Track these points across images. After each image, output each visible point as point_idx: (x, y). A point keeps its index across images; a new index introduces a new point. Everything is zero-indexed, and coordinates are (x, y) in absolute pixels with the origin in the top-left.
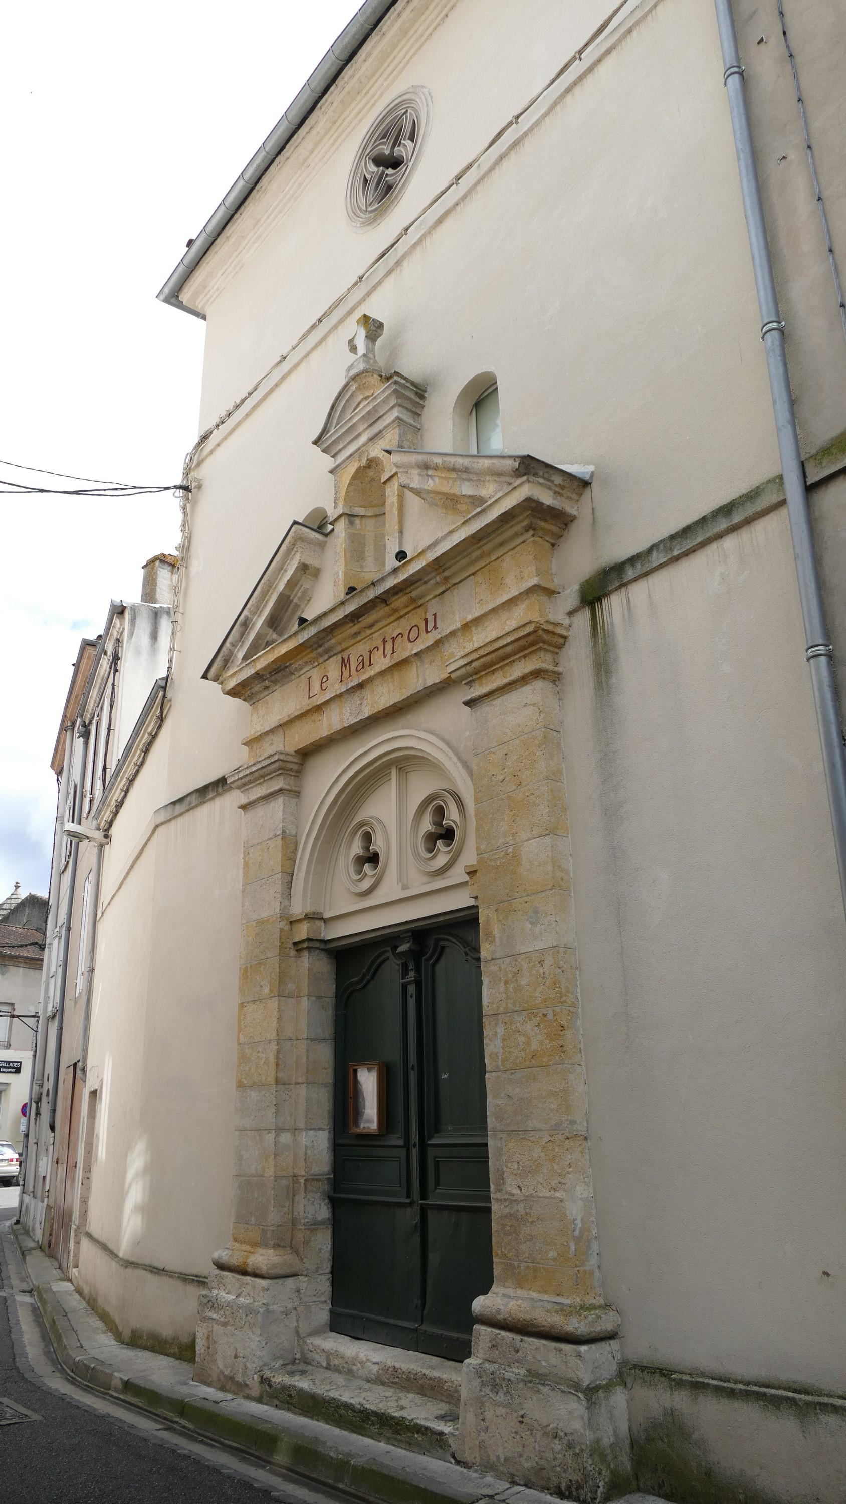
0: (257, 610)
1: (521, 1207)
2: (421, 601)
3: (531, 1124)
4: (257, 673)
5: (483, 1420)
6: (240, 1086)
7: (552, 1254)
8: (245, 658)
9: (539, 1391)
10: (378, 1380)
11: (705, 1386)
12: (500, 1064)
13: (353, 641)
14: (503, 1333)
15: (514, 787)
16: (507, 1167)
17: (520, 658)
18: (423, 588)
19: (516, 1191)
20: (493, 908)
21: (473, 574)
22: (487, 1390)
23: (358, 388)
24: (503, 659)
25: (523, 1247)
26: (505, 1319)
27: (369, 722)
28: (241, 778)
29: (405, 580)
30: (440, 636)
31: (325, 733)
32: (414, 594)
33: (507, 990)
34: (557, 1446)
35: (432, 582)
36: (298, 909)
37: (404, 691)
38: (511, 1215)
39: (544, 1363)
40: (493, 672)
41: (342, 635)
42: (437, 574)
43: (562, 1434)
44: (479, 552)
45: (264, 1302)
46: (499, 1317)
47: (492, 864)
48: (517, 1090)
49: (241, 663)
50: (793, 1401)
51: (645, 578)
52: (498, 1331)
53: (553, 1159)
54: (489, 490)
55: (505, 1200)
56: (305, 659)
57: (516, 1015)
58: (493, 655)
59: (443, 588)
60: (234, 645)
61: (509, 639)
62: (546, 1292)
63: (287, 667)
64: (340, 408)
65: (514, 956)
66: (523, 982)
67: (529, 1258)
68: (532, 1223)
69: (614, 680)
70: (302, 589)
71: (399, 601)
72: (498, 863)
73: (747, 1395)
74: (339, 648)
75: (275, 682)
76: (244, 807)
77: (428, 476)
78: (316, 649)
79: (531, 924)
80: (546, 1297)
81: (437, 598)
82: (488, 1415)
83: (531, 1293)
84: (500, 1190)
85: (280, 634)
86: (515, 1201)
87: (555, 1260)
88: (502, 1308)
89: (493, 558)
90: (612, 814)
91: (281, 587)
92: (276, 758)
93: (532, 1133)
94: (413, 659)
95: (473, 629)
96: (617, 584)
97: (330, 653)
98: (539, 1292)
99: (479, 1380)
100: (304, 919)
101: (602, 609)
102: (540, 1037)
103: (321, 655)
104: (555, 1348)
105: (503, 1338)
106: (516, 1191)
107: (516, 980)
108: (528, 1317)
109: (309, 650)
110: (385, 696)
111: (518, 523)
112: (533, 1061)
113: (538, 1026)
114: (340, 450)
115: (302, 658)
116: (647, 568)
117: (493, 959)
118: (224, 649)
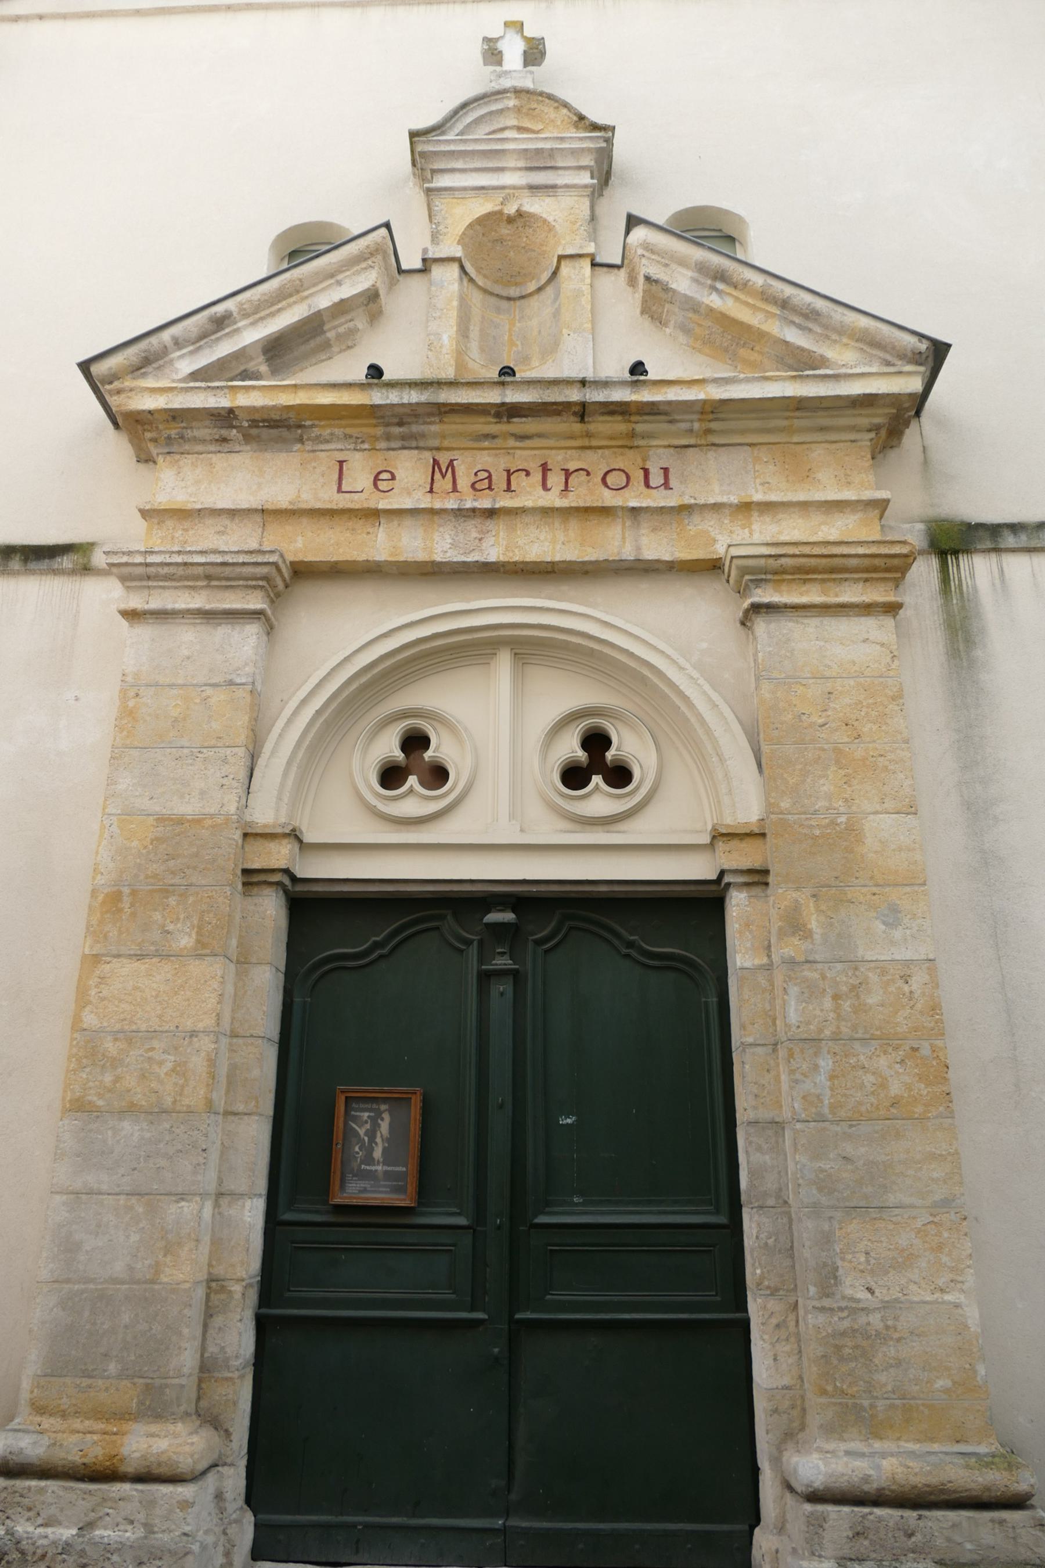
0: (257, 312)
2: (641, 443)
3: (891, 1199)
4: (231, 411)
6: (78, 1107)
8: (194, 376)
12: (826, 1111)
13: (471, 444)
14: (878, 1511)
15: (846, 740)
16: (843, 1259)
17: (859, 580)
18: (665, 426)
19: (863, 1295)
21: (750, 445)
23: (518, 110)
24: (833, 570)
26: (879, 1490)
28: (147, 565)
29: (653, 403)
30: (693, 501)
31: (359, 555)
32: (640, 428)
33: (837, 1009)
35: (683, 426)
36: (265, 813)
37: (590, 550)
38: (854, 1331)
39: (969, 1546)
40: (805, 581)
41: (460, 427)
42: (700, 420)
44: (785, 423)
45: (187, 1529)
46: (866, 1488)
47: (805, 831)
48: (863, 1150)
49: (183, 380)
51: (1027, 554)
53: (940, 1247)
54: (843, 356)
55: (841, 1309)
56: (348, 431)
57: (857, 1045)
58: (824, 561)
59: (692, 441)
60: (178, 343)
61: (861, 550)
62: (932, 1440)
63: (300, 426)
64: (469, 119)
65: (854, 964)
67: (894, 1392)
68: (899, 1340)
69: (978, 653)
70: (351, 325)
71: (602, 426)
72: (817, 832)
74: (436, 443)
75: (248, 438)
76: (132, 615)
77: (716, 290)
78: (387, 425)
79: (884, 923)
80: (936, 1447)
81: (672, 450)
83: (902, 1443)
85: (275, 372)
86: (863, 1309)
87: (947, 1391)
88: (872, 1472)
89: (795, 439)
90: (978, 812)
91: (324, 301)
92: (272, 559)
93: (897, 1211)
94: (620, 514)
95: (756, 514)
96: (989, 545)
97: (410, 442)
98: (919, 1441)
100: (286, 835)
101: (958, 565)
102: (907, 1079)
103: (388, 437)
104: (992, 1521)
105: (880, 1519)
106: (863, 1295)
107: (858, 996)
108: (934, 1480)
109: (374, 421)
110: (539, 545)
111: (868, 416)
112: (893, 1110)
113: (902, 1062)
114: (452, 170)
115: (345, 427)
116: (1034, 543)
117: (807, 962)
118: (153, 340)
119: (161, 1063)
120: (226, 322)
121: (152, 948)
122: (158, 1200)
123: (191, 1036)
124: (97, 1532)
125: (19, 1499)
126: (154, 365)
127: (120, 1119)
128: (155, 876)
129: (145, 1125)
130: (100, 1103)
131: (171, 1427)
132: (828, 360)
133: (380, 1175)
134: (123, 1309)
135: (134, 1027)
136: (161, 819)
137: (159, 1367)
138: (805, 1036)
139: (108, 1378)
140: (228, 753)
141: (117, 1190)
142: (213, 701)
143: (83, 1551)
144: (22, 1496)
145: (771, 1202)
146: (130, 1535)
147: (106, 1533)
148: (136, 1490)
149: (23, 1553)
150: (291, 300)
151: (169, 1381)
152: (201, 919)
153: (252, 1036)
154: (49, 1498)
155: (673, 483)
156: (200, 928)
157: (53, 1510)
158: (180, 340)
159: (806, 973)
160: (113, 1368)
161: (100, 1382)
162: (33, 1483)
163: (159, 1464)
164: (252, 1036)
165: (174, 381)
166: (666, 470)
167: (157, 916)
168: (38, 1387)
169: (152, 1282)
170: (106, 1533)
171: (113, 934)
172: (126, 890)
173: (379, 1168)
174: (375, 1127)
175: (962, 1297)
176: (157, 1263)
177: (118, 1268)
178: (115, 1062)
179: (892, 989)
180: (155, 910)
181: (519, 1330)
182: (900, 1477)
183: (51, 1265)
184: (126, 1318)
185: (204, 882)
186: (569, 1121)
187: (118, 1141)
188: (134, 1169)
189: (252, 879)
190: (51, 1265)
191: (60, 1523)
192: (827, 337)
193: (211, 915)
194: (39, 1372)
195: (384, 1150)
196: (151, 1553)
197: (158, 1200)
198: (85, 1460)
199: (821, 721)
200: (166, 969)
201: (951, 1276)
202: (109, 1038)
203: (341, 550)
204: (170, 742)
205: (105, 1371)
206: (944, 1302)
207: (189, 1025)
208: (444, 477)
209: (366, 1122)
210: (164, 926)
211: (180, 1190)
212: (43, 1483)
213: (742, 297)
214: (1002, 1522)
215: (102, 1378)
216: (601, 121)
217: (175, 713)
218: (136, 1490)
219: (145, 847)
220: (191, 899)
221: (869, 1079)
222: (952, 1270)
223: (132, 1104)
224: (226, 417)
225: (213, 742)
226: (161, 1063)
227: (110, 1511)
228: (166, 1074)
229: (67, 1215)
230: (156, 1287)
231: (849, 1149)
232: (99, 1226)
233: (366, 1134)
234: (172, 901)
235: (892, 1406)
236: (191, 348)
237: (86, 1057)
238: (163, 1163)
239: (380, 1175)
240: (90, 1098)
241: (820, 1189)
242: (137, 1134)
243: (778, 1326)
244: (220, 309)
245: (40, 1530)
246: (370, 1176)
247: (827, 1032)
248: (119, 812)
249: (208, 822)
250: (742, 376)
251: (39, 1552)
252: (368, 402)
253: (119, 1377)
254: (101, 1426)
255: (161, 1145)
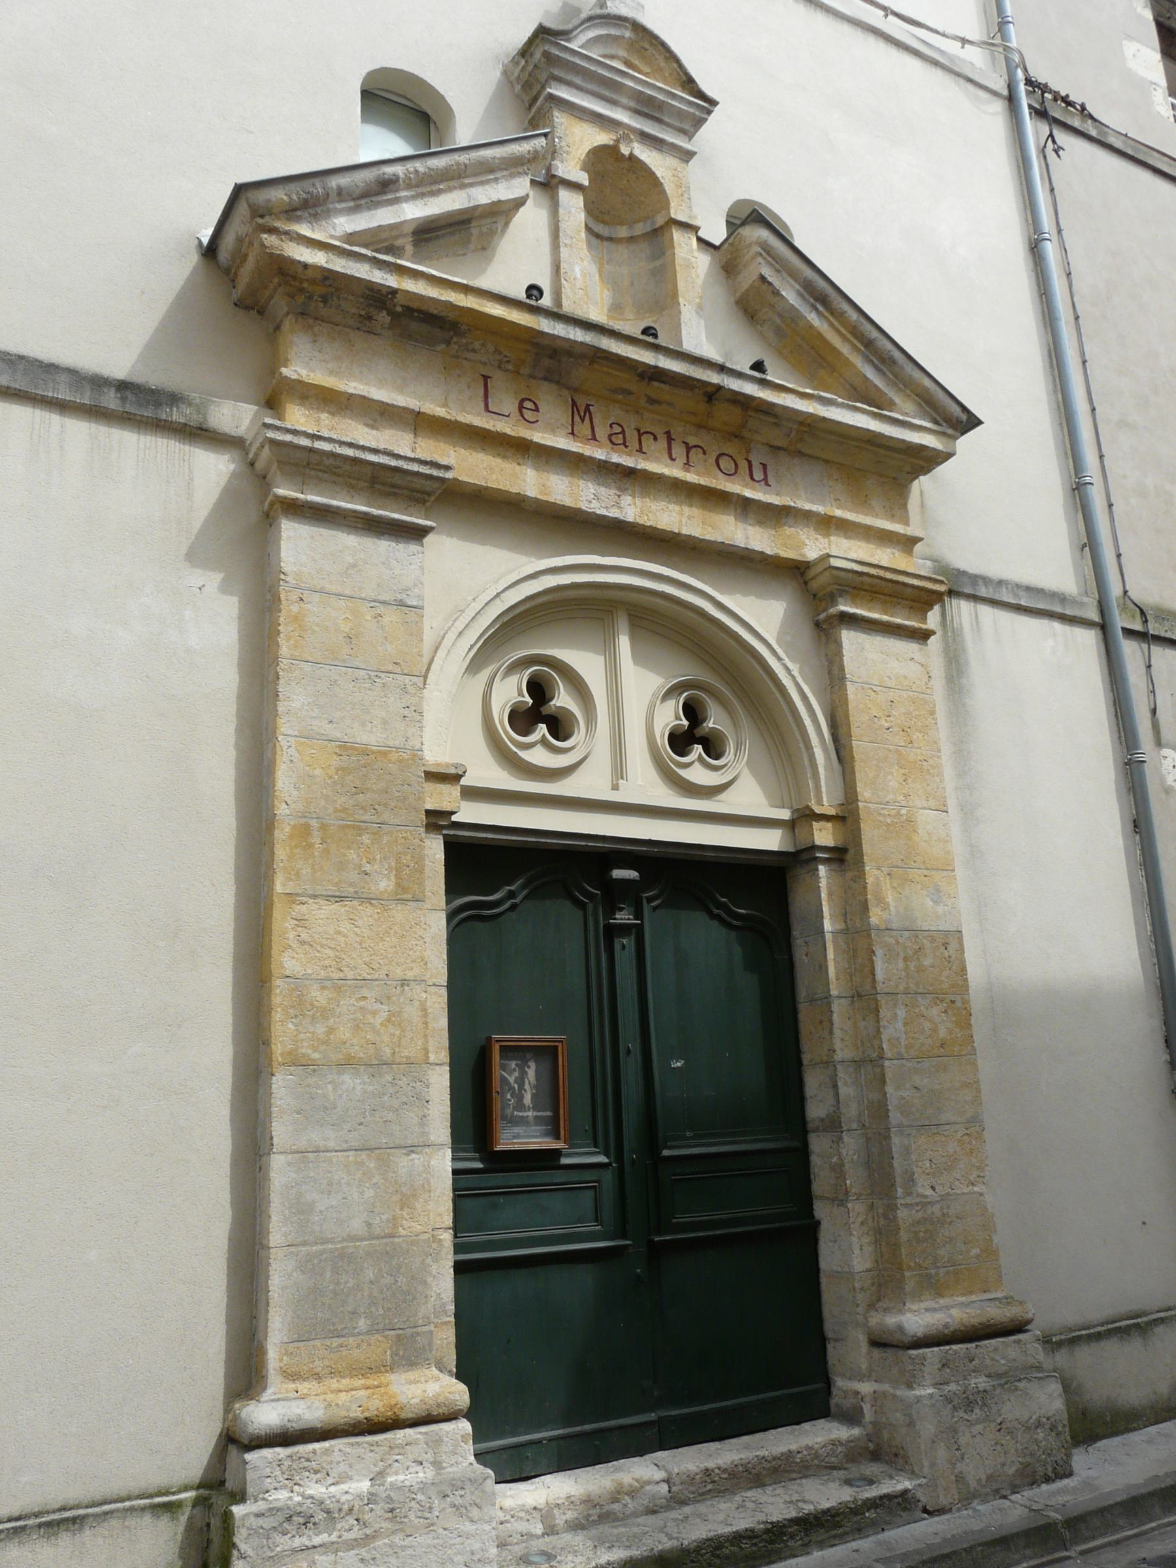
1: (936, 1209)
3: (944, 1118)
5: (958, 1449)
7: (975, 1251)
9: (1017, 1389)
10: (676, 1501)
11: (1079, 1337)
12: (903, 1050)
14: (954, 1347)
19: (929, 1192)
20: (886, 870)
22: (961, 1414)
25: (941, 1252)
27: (111, 400)
33: (907, 968)
34: (1040, 1434)
38: (925, 1219)
39: (1003, 1362)
43: (1044, 1420)
46: (946, 1331)
47: (881, 818)
48: (926, 1081)
50: (1137, 1325)
52: (947, 1347)
55: (917, 1204)
57: (919, 998)
60: (341, 194)
61: (916, 582)
62: (971, 1293)
66: (927, 962)
68: (950, 1223)
69: (964, 681)
72: (889, 821)
73: (1109, 1333)
79: (932, 900)
80: (974, 1298)
82: (963, 1441)
84: (910, 1194)
87: (978, 1256)
98: (963, 1295)
99: (950, 1406)
102: (949, 1025)
105: (956, 1352)
107: (918, 959)
113: (946, 1012)
119: (374, 1013)
120: (391, 187)
121: (351, 890)
122: (389, 1154)
123: (402, 985)
124: (389, 1479)
125: (306, 1464)
126: (311, 211)
127: (339, 1073)
128: (344, 810)
129: (366, 1078)
130: (316, 1056)
131: (427, 1372)
132: (895, 404)
133: (531, 1119)
134: (366, 1265)
135: (341, 975)
136: (345, 748)
137: (409, 1317)
138: (887, 990)
139: (359, 1334)
140: (407, 681)
141: (345, 1146)
142: (386, 620)
143: (389, 1497)
144: (308, 1460)
145: (855, 1126)
146: (425, 1474)
147: (401, 1477)
148: (420, 1433)
149: (328, 1512)
150: (452, 183)
151: (420, 1329)
152: (398, 861)
153: (434, 985)
154: (337, 1457)
155: (771, 481)
156: (398, 871)
157: (342, 1467)
158: (344, 192)
159: (886, 939)
160: (362, 1324)
161: (351, 1339)
162: (316, 1446)
163: (438, 1406)
164: (434, 985)
165: (332, 237)
166: (764, 466)
167: (352, 855)
168: (286, 1354)
169: (392, 1236)
170: (401, 1477)
171: (306, 871)
172: (314, 823)
173: (530, 1114)
174: (523, 1074)
175: (984, 1187)
176: (394, 1218)
177: (357, 1225)
178: (325, 1013)
179: (938, 954)
180: (349, 848)
181: (655, 1252)
182: (965, 1321)
183: (284, 1229)
184: (370, 1274)
185: (396, 821)
186: (679, 1064)
187: (340, 1095)
188: (361, 1124)
189: (436, 820)
190: (284, 1229)
191: (351, 1478)
192: (896, 385)
193: (409, 858)
194: (286, 1340)
195: (533, 1096)
196: (453, 1485)
197: (389, 1154)
198: (367, 1414)
199: (887, 725)
200: (367, 914)
201: (978, 1173)
202: (316, 986)
203: (494, 477)
204: (344, 661)
205: (355, 1328)
206: (975, 1193)
207: (399, 972)
208: (583, 420)
209: (515, 1070)
210: (360, 866)
211: (410, 1142)
212: (326, 1444)
213: (836, 323)
214: (1019, 1341)
215: (353, 1335)
216: (710, 93)
217: (345, 628)
218: (420, 1433)
219: (330, 777)
220: (385, 839)
221: (927, 1025)
222: (978, 1168)
223: (350, 1057)
224: (380, 297)
225: (390, 667)
226: (374, 1013)
227: (398, 1457)
228: (381, 1024)
229: (293, 1175)
230: (396, 1240)
231: (917, 1080)
232: (330, 1184)
233: (515, 1082)
234: (366, 839)
235: (947, 1272)
236: (351, 204)
237: (292, 1007)
238: (390, 1116)
239: (531, 1119)
240: (303, 1051)
241: (902, 1113)
242: (359, 1088)
243: (862, 1223)
244: (389, 170)
245: (332, 1489)
246: (522, 1121)
247: (901, 988)
248: (296, 733)
249: (394, 756)
250: (840, 400)
251: (346, 1507)
252: (535, 327)
253: (369, 1332)
254: (360, 1382)
255: (386, 1098)
